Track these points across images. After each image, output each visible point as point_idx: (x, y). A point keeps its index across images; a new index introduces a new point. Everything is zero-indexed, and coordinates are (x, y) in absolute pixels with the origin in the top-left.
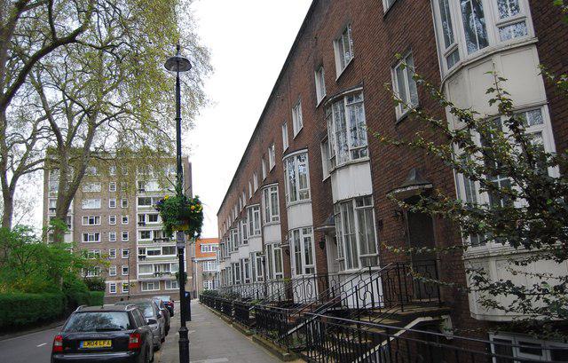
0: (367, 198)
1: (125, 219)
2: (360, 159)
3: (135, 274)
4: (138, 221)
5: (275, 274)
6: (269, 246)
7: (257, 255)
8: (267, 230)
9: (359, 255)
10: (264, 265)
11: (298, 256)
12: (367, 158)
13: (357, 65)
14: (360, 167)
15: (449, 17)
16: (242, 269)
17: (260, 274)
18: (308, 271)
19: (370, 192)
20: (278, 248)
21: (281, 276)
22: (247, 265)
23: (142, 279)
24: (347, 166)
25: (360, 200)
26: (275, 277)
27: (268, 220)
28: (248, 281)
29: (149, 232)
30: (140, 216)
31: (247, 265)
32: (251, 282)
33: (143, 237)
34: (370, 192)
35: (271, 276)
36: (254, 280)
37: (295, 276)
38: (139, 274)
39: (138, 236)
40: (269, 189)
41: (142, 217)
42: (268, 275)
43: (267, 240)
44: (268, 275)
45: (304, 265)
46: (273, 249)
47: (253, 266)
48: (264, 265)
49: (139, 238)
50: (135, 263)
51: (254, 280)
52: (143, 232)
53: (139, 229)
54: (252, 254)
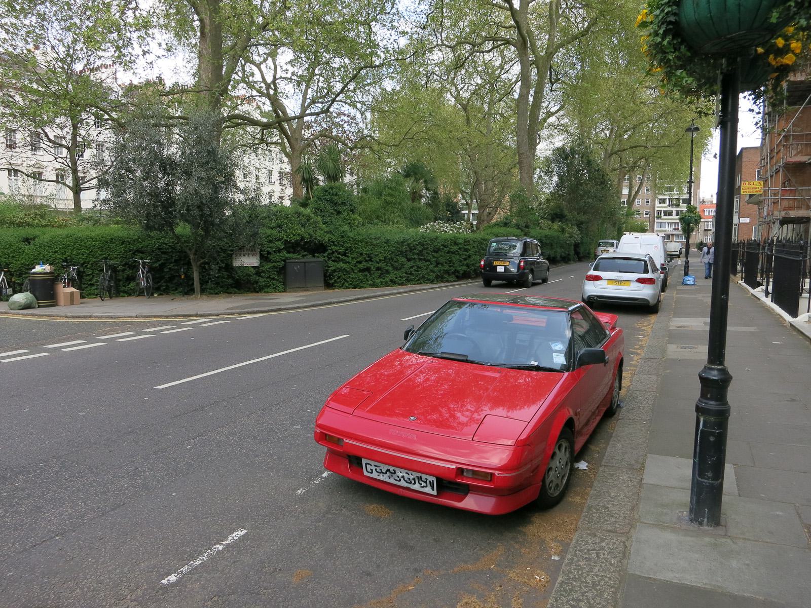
1: (647, 202)
29: (665, 199)
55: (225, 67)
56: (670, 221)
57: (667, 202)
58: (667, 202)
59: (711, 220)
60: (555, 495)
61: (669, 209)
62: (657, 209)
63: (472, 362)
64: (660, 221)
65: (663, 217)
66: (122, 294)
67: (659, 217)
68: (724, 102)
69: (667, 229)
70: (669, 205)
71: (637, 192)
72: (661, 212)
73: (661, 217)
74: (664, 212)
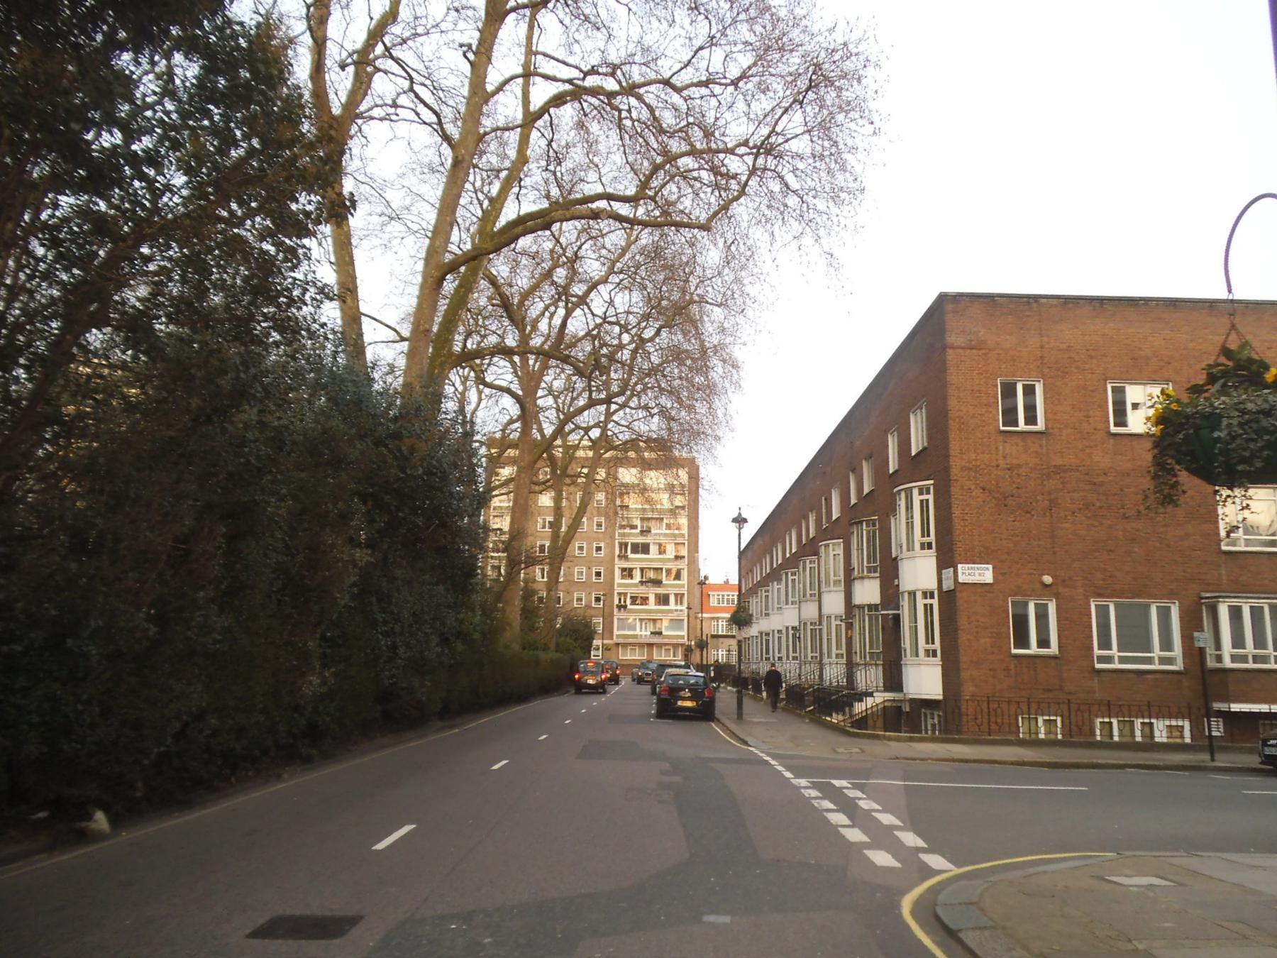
0: (876, 606)
1: (599, 549)
2: (872, 575)
3: (612, 632)
4: (617, 552)
5: (810, 655)
6: (805, 624)
7: (811, 624)
8: (825, 598)
9: (867, 651)
10: (800, 642)
11: (829, 640)
12: (878, 575)
13: (900, 473)
14: (872, 580)
15: (912, 508)
16: (787, 641)
17: (795, 651)
18: (837, 656)
19: (878, 602)
20: (839, 623)
21: (816, 657)
22: (779, 638)
23: (621, 641)
24: (862, 578)
25: (871, 607)
26: (810, 659)
27: (828, 584)
28: (780, 659)
29: (631, 570)
30: (621, 544)
31: (779, 638)
32: (784, 659)
33: (623, 577)
34: (878, 602)
35: (806, 656)
36: (788, 658)
37: (826, 660)
38: (616, 632)
39: (617, 573)
40: (915, 492)
41: (623, 546)
42: (802, 655)
43: (826, 611)
44: (802, 655)
45: (791, 654)
46: (809, 627)
47: (787, 641)
48: (800, 642)
49: (618, 580)
50: (612, 615)
51: (788, 658)
52: (624, 570)
53: (619, 564)
54: (761, 633)
55: (236, 208)
56: (644, 616)
57: (637, 574)
58: (637, 574)
59: (1138, 722)
60: (889, 436)
61: (641, 591)
62: (617, 590)
63: (369, 10)
64: (623, 615)
65: (629, 607)
66: (319, 284)
67: (622, 607)
68: (950, 348)
69: (638, 632)
70: (642, 583)
71: (575, 525)
72: (625, 594)
73: (625, 607)
74: (631, 597)
